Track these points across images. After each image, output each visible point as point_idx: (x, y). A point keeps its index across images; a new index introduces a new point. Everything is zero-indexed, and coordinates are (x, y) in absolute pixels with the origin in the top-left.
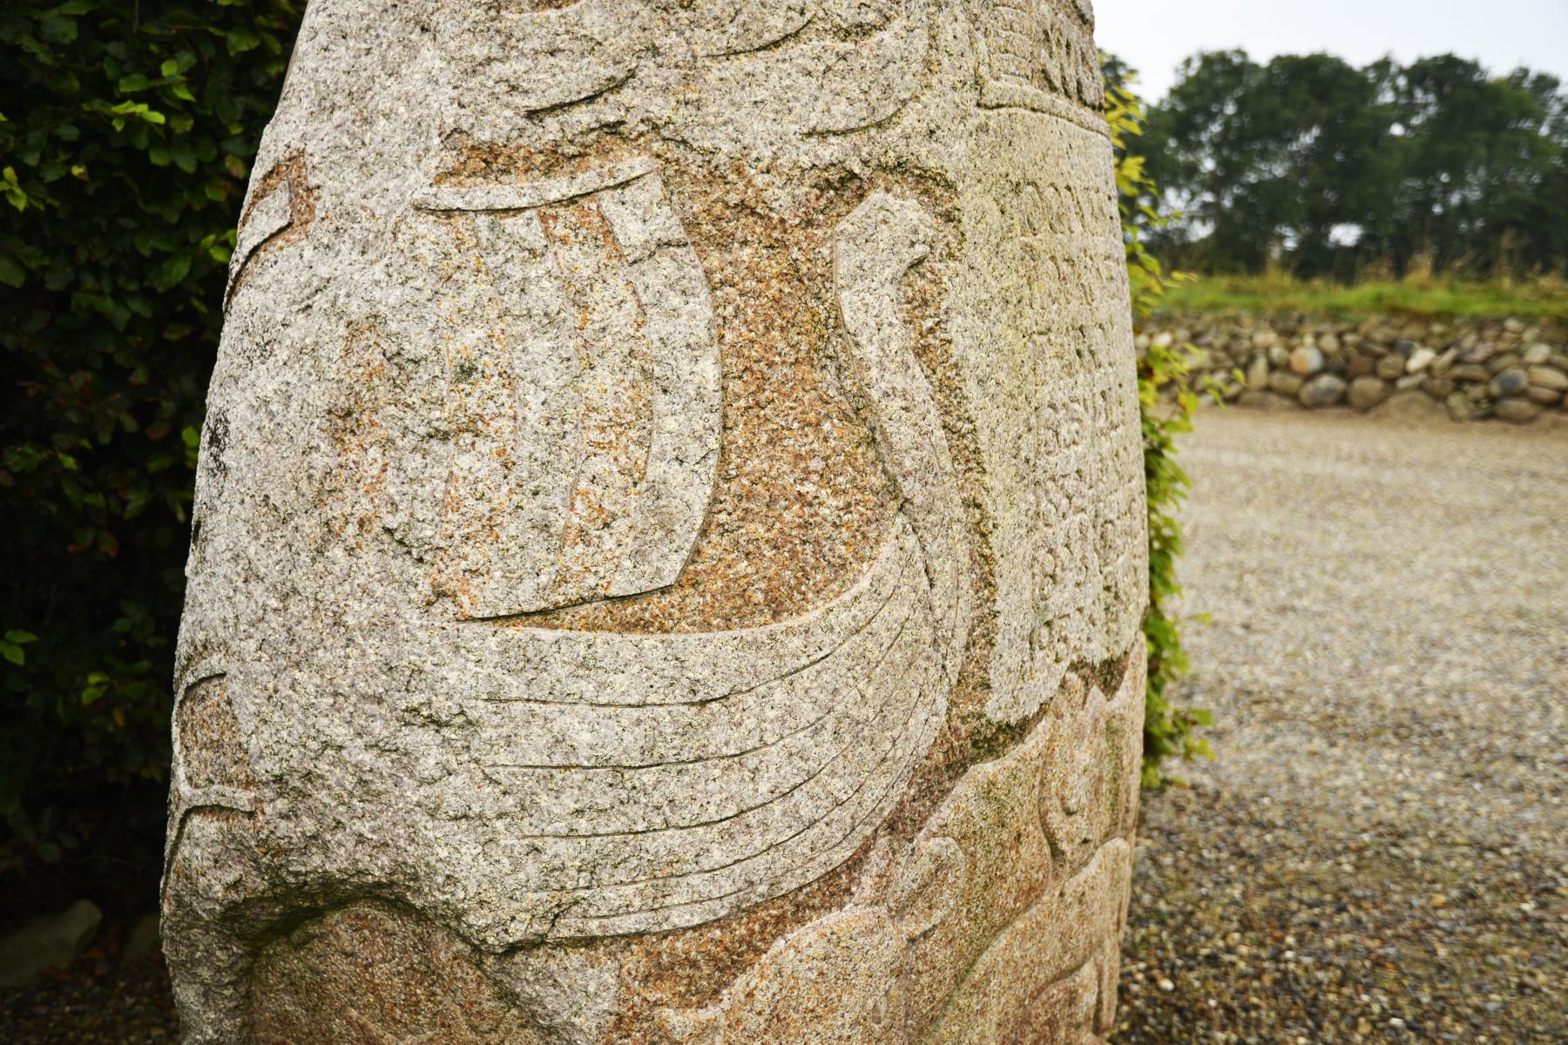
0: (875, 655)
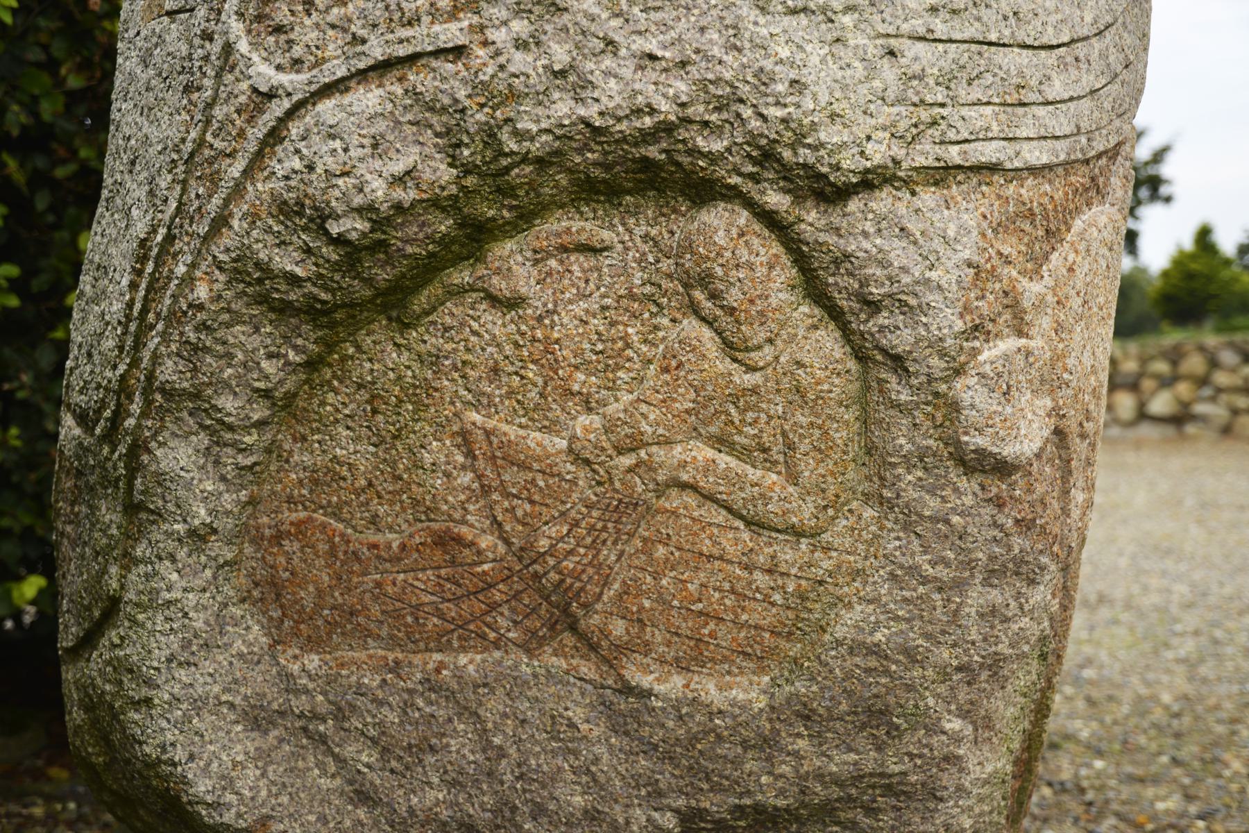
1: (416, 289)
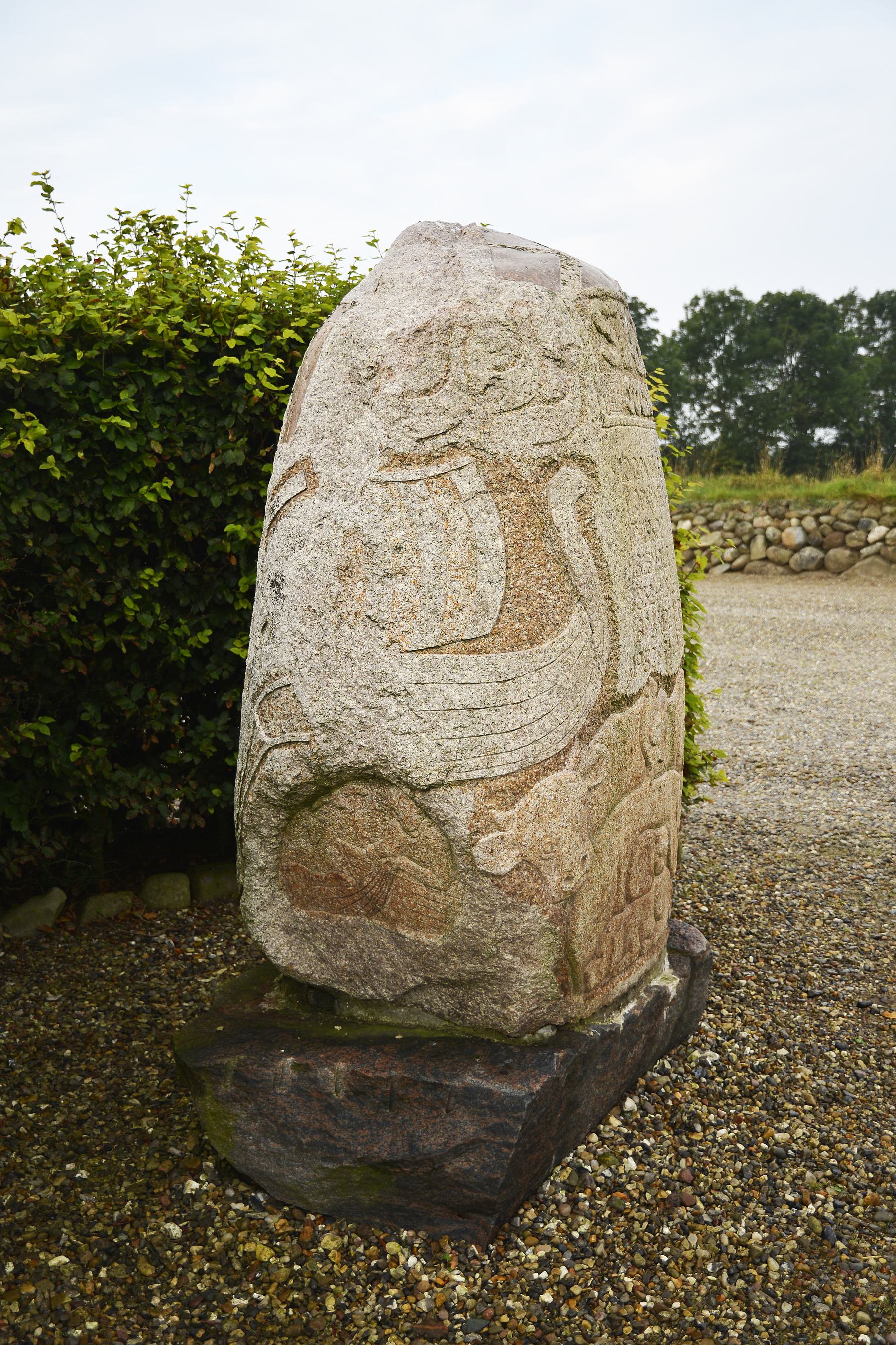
0: (572, 661)
1: (314, 802)
